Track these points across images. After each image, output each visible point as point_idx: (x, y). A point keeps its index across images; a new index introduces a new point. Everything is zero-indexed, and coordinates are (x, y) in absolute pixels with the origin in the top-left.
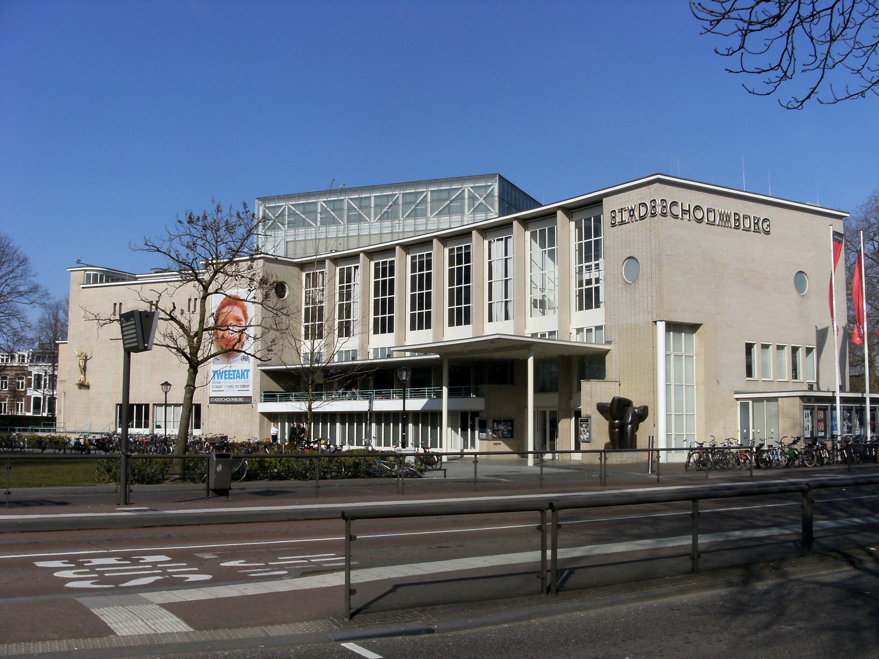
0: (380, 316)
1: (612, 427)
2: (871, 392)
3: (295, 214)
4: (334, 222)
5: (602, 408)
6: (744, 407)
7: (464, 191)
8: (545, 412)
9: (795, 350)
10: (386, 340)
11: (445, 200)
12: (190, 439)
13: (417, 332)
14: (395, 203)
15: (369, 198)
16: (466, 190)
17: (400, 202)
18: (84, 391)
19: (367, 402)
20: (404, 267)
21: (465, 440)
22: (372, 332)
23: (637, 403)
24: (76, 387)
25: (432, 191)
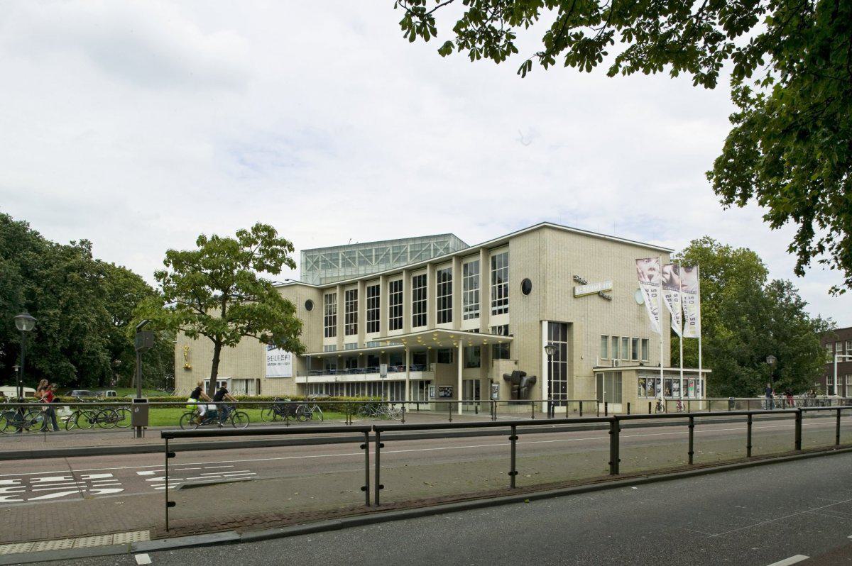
0: (447, 309)
1: (512, 389)
2: (679, 367)
3: (325, 261)
4: (349, 265)
5: (506, 378)
6: (600, 377)
7: (430, 245)
8: (472, 381)
9: (635, 342)
10: (352, 339)
11: (418, 251)
12: (164, 335)
13: (328, 338)
14: (388, 254)
15: (372, 249)
16: (432, 245)
17: (391, 252)
18: (188, 373)
19: (565, 407)
20: (362, 299)
21: (397, 395)
22: (324, 335)
23: (530, 373)
24: (177, 503)
25: (411, 245)
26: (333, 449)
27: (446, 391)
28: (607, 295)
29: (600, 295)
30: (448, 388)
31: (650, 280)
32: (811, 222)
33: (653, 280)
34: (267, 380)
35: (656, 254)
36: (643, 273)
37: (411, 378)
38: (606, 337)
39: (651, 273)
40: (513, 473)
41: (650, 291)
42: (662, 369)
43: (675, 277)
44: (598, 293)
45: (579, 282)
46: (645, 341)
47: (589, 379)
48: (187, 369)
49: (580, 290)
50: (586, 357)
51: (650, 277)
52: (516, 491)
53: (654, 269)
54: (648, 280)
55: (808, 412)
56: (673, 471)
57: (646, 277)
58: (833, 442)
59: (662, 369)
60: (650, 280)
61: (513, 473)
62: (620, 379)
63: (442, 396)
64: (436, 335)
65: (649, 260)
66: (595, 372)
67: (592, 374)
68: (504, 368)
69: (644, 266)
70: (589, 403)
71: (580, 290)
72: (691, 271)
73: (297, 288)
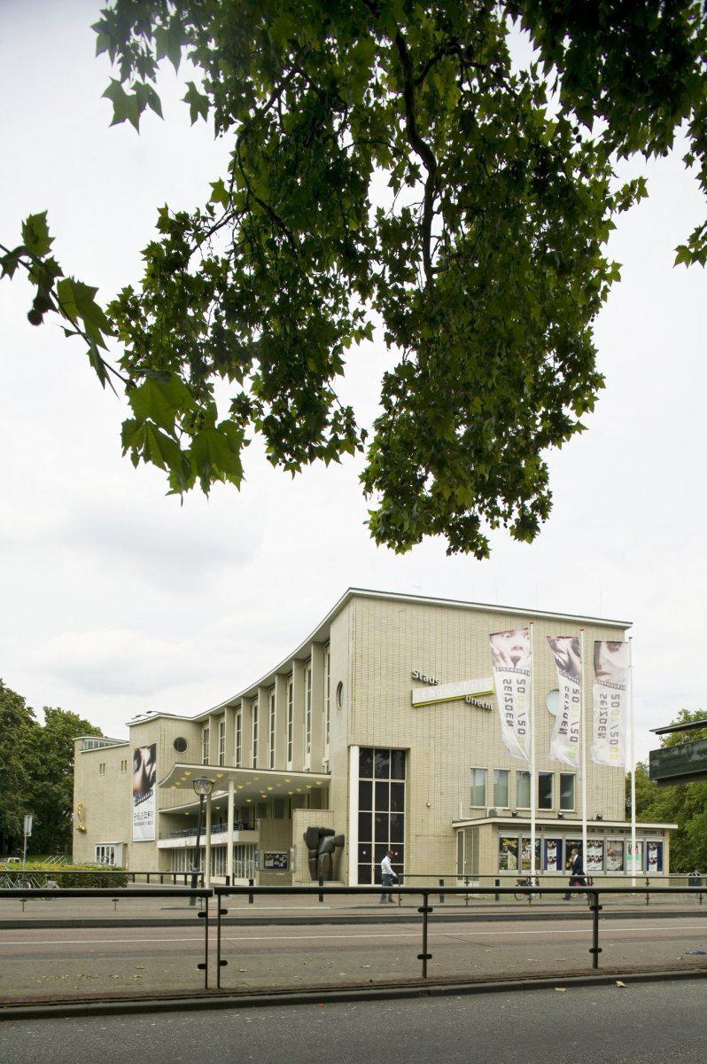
6: (460, 834)
9: (545, 781)
26: (186, 933)
27: (278, 860)
28: (481, 702)
29: (473, 703)
30: (281, 855)
31: (515, 664)
32: (560, 412)
33: (519, 665)
34: (135, 845)
35: (526, 623)
36: (502, 655)
37: (212, 843)
38: (506, 772)
39: (516, 653)
40: (596, 951)
41: (571, 691)
42: (585, 824)
43: (575, 659)
44: (463, 699)
45: (424, 682)
46: (567, 781)
47: (444, 840)
48: (83, 832)
49: (422, 694)
50: (432, 807)
51: (515, 660)
52: (597, 971)
53: (521, 648)
54: (511, 665)
55: (449, 900)
56: (530, 978)
57: (508, 659)
58: (202, 985)
59: (585, 824)
60: (515, 664)
61: (596, 951)
62: (477, 837)
63: (270, 867)
64: (188, 774)
65: (512, 633)
66: (456, 828)
67: (450, 832)
68: (304, 820)
69: (502, 644)
70: (168, 876)
71: (422, 694)
72: (617, 650)
73: (162, 721)
